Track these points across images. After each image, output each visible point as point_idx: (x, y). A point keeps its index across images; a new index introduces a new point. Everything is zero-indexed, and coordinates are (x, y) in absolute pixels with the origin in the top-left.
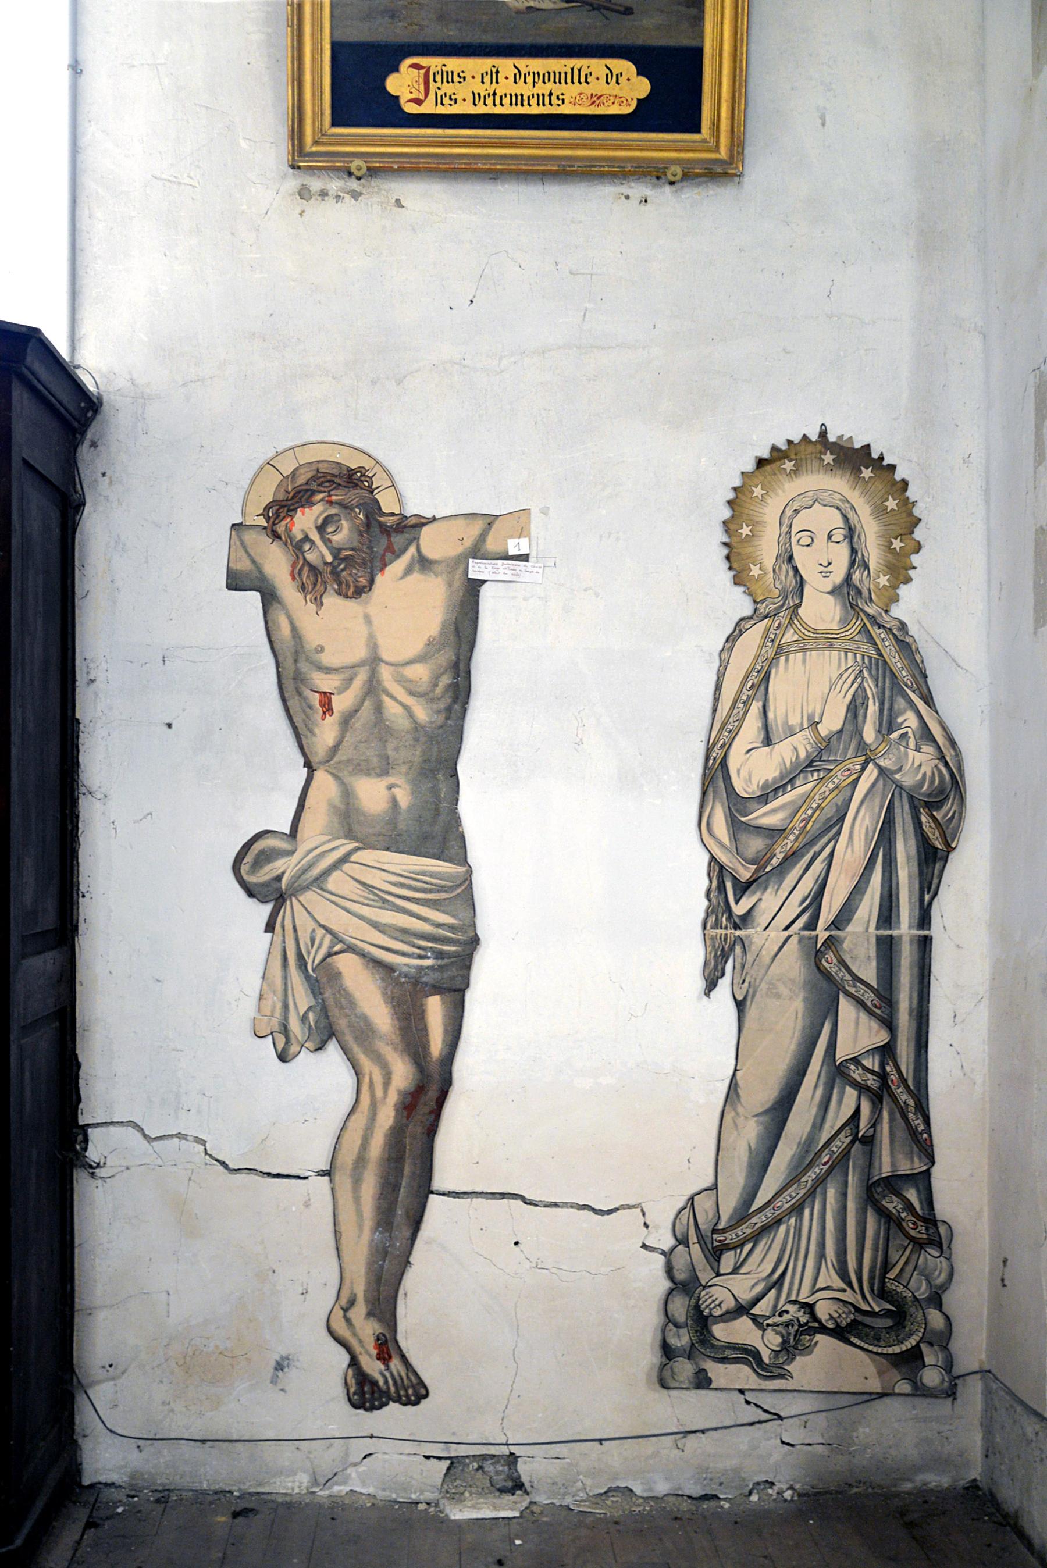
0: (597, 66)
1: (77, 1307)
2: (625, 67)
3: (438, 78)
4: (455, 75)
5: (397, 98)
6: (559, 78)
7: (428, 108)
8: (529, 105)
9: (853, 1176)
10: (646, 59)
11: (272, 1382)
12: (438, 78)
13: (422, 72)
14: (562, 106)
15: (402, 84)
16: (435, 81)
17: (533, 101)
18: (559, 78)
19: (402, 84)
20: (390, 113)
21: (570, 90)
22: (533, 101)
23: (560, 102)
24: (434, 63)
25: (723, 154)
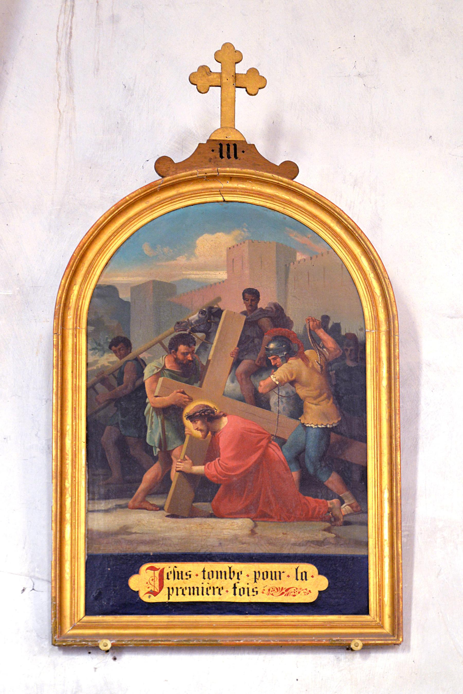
0: (288, 568)
1: (326, 334)
2: (311, 569)
3: (171, 576)
4: (184, 574)
5: (320, 592)
6: (220, 575)
7: (162, 598)
8: (208, 594)
9: (117, 276)
10: (324, 564)
11: (219, 312)
12: (171, 576)
13: (157, 573)
14: (257, 596)
15: (141, 582)
16: (168, 579)
17: (210, 592)
18: (220, 575)
19: (141, 582)
20: (133, 605)
21: (228, 584)
22: (210, 592)
23: (255, 593)
24: (168, 567)
25: (387, 628)
